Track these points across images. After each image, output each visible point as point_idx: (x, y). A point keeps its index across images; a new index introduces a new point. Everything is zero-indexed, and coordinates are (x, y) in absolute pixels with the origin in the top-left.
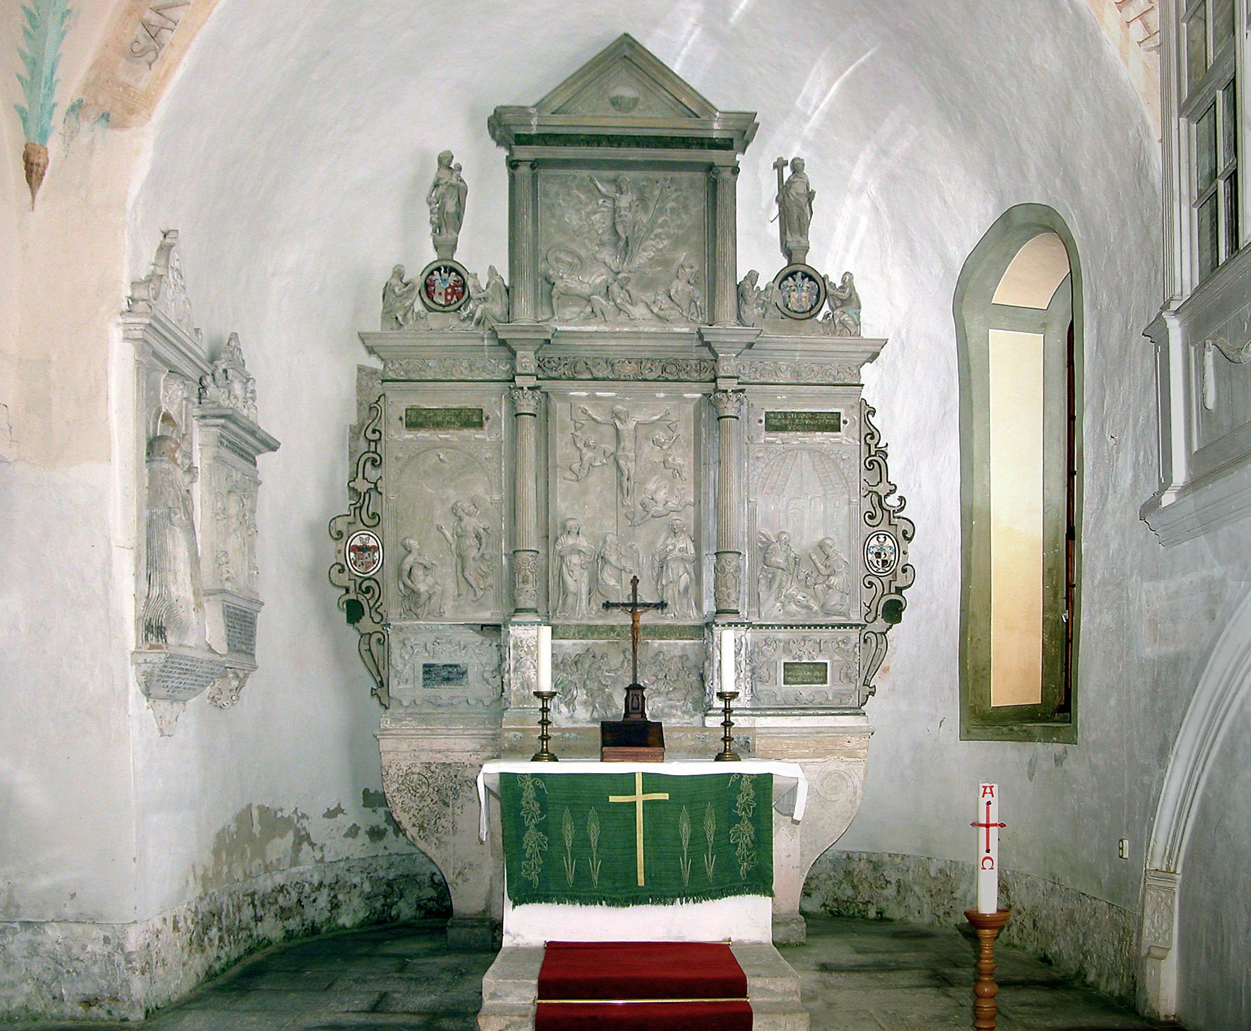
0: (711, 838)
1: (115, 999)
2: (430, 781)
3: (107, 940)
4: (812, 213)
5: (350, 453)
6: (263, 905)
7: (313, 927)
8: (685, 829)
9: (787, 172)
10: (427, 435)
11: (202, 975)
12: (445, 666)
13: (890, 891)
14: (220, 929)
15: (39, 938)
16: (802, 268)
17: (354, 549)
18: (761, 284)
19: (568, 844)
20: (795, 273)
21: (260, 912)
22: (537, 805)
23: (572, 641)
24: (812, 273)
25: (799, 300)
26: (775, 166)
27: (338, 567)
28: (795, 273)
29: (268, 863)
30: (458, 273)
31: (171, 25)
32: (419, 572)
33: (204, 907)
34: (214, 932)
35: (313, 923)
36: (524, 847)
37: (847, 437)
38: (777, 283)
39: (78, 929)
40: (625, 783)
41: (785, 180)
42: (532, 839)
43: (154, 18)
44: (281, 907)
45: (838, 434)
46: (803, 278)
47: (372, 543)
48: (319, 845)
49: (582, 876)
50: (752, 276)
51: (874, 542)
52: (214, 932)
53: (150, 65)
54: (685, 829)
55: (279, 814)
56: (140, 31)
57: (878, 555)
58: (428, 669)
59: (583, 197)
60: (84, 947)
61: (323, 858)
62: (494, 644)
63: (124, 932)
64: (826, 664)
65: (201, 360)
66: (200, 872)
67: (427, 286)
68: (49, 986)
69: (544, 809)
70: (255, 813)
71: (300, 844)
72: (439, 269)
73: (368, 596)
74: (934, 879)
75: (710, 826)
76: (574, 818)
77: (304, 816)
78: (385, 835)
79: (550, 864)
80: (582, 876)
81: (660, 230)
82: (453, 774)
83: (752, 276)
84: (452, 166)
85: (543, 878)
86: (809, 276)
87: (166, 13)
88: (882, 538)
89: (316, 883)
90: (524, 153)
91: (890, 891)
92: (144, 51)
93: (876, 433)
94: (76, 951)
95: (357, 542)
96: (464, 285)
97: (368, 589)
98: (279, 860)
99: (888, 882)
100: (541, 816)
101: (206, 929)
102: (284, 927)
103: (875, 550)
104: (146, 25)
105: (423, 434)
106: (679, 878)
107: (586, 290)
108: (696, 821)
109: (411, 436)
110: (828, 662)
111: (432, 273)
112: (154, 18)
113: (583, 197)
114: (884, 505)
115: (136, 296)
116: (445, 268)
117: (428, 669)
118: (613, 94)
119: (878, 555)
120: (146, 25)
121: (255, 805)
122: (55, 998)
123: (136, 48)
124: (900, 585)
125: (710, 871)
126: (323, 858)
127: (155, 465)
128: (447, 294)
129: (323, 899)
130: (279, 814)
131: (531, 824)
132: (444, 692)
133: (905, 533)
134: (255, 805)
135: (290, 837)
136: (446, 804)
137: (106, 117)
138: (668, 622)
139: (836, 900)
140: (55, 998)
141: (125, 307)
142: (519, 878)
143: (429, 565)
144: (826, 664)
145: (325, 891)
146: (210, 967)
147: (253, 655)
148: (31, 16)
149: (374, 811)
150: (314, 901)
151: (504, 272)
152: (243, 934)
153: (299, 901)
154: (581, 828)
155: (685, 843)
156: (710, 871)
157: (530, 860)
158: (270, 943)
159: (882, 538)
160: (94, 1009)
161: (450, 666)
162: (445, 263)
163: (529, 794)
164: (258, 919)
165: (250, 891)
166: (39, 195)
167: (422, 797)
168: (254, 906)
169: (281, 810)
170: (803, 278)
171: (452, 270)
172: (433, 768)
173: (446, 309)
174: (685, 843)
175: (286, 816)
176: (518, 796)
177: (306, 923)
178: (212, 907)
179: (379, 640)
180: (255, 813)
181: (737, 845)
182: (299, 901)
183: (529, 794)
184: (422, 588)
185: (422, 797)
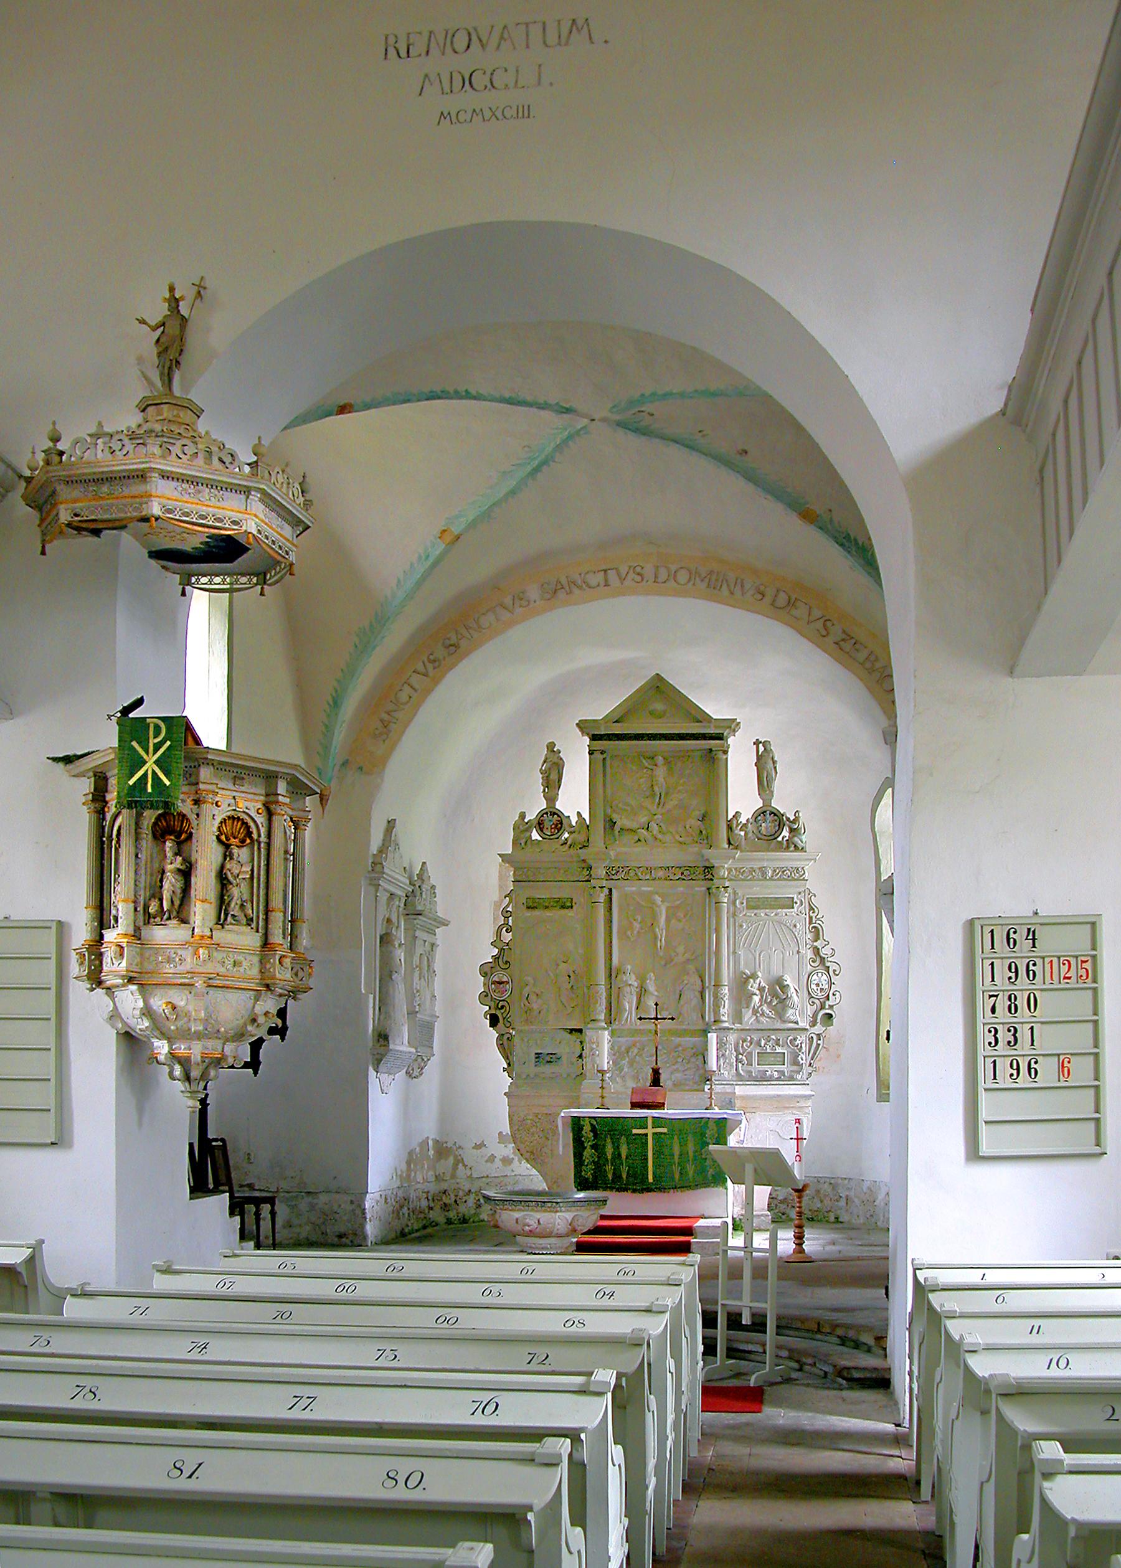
0: (691, 1154)
1: (355, 1234)
2: (538, 1124)
3: (352, 1202)
4: (776, 773)
5: (494, 918)
6: (433, 1201)
7: (464, 1218)
8: (676, 1150)
9: (761, 748)
10: (538, 913)
11: (399, 1233)
12: (548, 1054)
13: (842, 1203)
14: (409, 1209)
15: (315, 1201)
16: (770, 808)
17: (494, 983)
18: (743, 820)
19: (609, 1157)
20: (765, 812)
21: (432, 1205)
22: (592, 1134)
23: (626, 1039)
24: (775, 812)
25: (766, 828)
26: (754, 743)
27: (485, 994)
28: (765, 812)
29: (437, 1174)
30: (559, 816)
31: (395, 721)
32: (533, 997)
33: (400, 1194)
34: (405, 1209)
35: (464, 1216)
36: (584, 1158)
37: (796, 916)
38: (754, 818)
39: (337, 1196)
40: (642, 1122)
41: (760, 753)
42: (588, 1153)
43: (385, 716)
44: (444, 1203)
45: (792, 910)
46: (770, 815)
47: (505, 979)
48: (469, 1166)
49: (617, 1176)
50: (737, 815)
51: (815, 977)
52: (405, 1209)
53: (384, 741)
54: (676, 1150)
55: (445, 1145)
56: (380, 725)
57: (817, 985)
58: (538, 1055)
59: (634, 768)
60: (340, 1206)
61: (471, 1174)
62: (579, 1040)
63: (618, 814)
64: (784, 1053)
65: (406, 885)
66: (399, 1173)
67: (539, 824)
68: (319, 1228)
69: (596, 1136)
70: (431, 1143)
71: (457, 1165)
72: (547, 813)
73: (502, 1011)
74: (865, 1193)
75: (691, 1147)
76: (613, 1143)
77: (460, 1147)
78: (512, 1162)
79: (599, 1167)
80: (617, 1176)
81: (681, 788)
82: (552, 1120)
83: (737, 815)
84: (555, 750)
85: (595, 1177)
86: (775, 813)
87: (392, 713)
88: (820, 974)
89: (467, 1190)
90: (598, 744)
91: (842, 1203)
92: (381, 734)
93: (816, 909)
94: (335, 1208)
95: (496, 979)
96: (561, 823)
97: (502, 1007)
98: (444, 1173)
99: (841, 1197)
100: (594, 1140)
101: (402, 1207)
102: (446, 1216)
103: (816, 982)
104: (382, 721)
105: (536, 913)
106: (672, 1178)
107: (635, 826)
108: (683, 1144)
109: (529, 914)
110: (786, 1052)
111: (542, 816)
112: (385, 716)
113: (634, 768)
114: (821, 954)
115: (376, 861)
116: (551, 812)
117: (538, 1055)
118: (651, 708)
119: (817, 985)
120: (382, 721)
121: (431, 1137)
122: (323, 1233)
123: (377, 732)
124: (831, 1004)
125: (691, 1173)
126: (471, 1174)
127: (383, 949)
128: (552, 828)
129: (471, 1200)
130: (445, 1145)
131: (587, 1145)
132: (548, 1069)
133: (834, 971)
134: (431, 1137)
135: (451, 1159)
136: (547, 1139)
137: (361, 768)
138: (684, 1027)
139: (810, 1210)
140: (323, 1233)
141: (370, 869)
142: (581, 1176)
143: (539, 993)
144: (784, 1053)
145: (473, 1196)
146: (403, 1229)
147: (432, 1048)
148: (326, 726)
149: (505, 1146)
150: (465, 1202)
151: (586, 815)
152: (422, 1216)
153: (456, 1201)
154: (617, 1148)
155: (676, 1157)
156: (691, 1173)
157: (587, 1165)
158: (437, 1225)
159: (820, 974)
160: (344, 1239)
161: (552, 1054)
162: (551, 810)
163: (587, 1128)
164: (431, 1208)
165: (426, 1190)
166: (327, 808)
167: (533, 1134)
168: (428, 1200)
169: (446, 1143)
170: (770, 815)
171: (555, 814)
172: (540, 1116)
173: (552, 837)
174: (676, 1157)
175: (449, 1146)
176: (581, 1129)
177: (459, 1215)
178: (405, 1195)
179: (508, 1038)
180: (431, 1143)
181: (706, 1159)
182: (456, 1201)
183: (587, 1128)
184: (535, 1006)
185: (533, 1134)
